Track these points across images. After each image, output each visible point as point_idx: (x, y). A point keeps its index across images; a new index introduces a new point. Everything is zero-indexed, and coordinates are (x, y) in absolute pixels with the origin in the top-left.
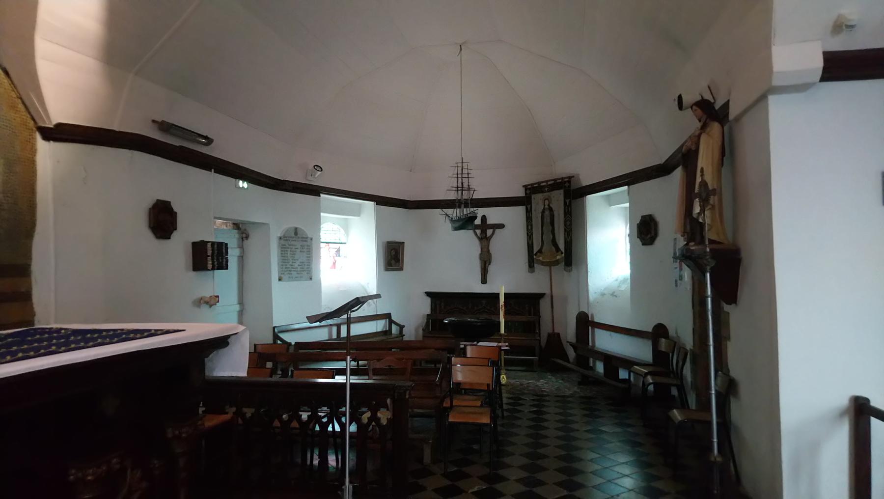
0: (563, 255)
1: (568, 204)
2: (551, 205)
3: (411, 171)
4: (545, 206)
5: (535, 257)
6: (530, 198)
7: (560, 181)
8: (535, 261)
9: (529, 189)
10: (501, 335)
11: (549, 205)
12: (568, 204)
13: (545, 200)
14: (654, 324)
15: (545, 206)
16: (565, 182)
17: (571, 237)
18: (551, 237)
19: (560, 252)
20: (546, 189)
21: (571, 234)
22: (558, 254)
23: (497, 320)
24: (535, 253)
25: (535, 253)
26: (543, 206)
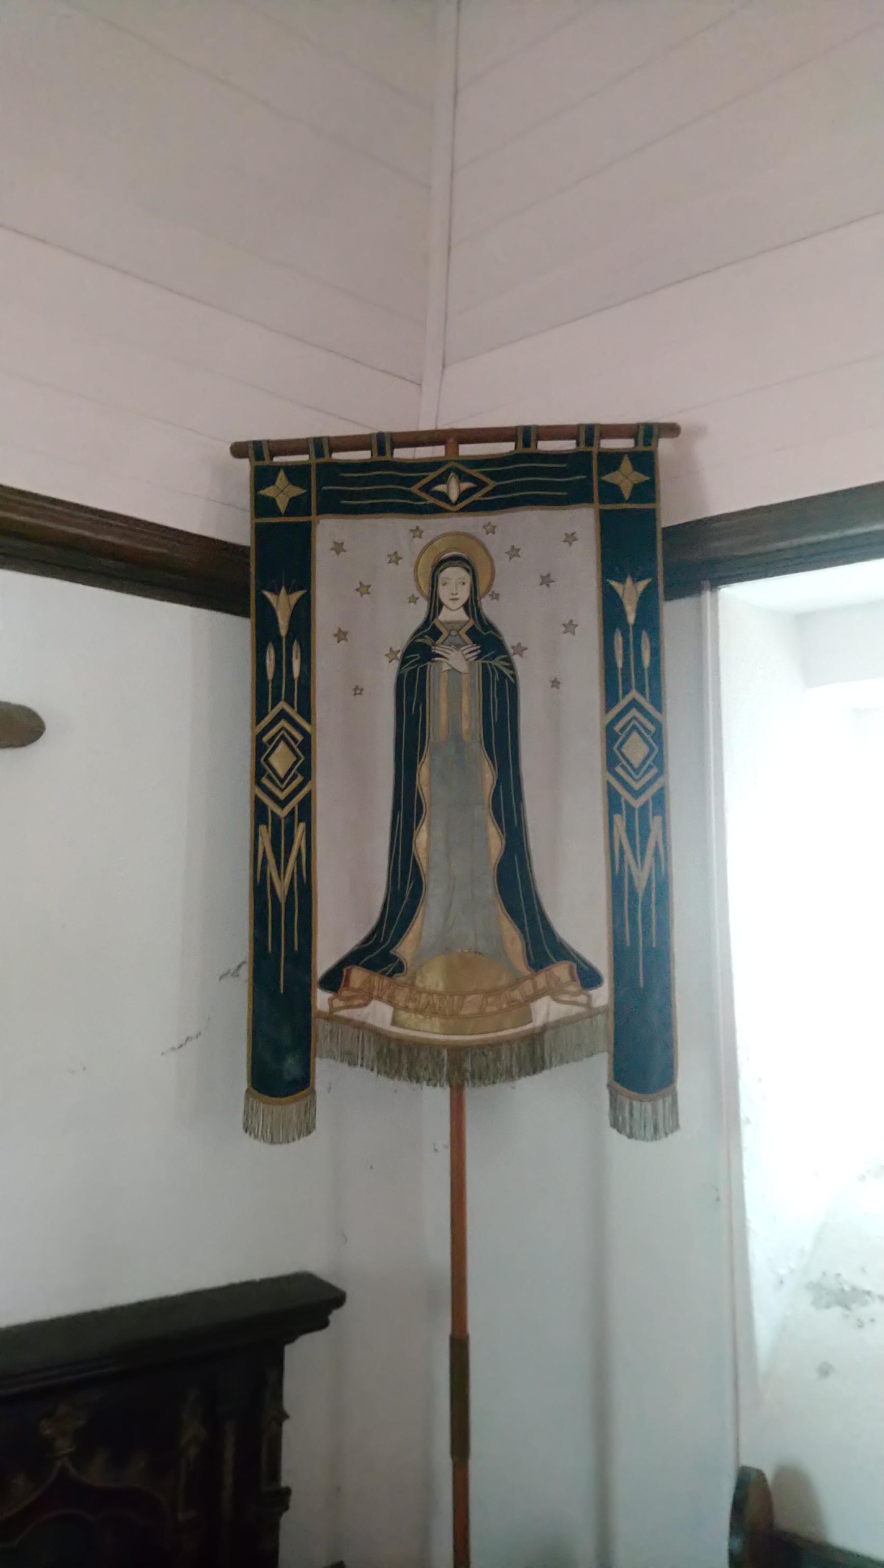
0: (602, 996)
1: (631, 618)
2: (488, 607)
3: (476, 952)
4: (435, 606)
5: (322, 999)
6: (305, 534)
7: (568, 445)
8: (320, 1029)
9: (296, 474)
10: (321, 488)
11: (472, 607)
12: (631, 618)
13: (440, 565)
14: (46, 731)
15: (435, 606)
16: (611, 460)
17: (662, 859)
18: (496, 844)
19: (561, 971)
20: (453, 489)
21: (655, 823)
22: (541, 979)
23: (375, 436)
24: (323, 964)
25: (323, 964)
26: (421, 609)
